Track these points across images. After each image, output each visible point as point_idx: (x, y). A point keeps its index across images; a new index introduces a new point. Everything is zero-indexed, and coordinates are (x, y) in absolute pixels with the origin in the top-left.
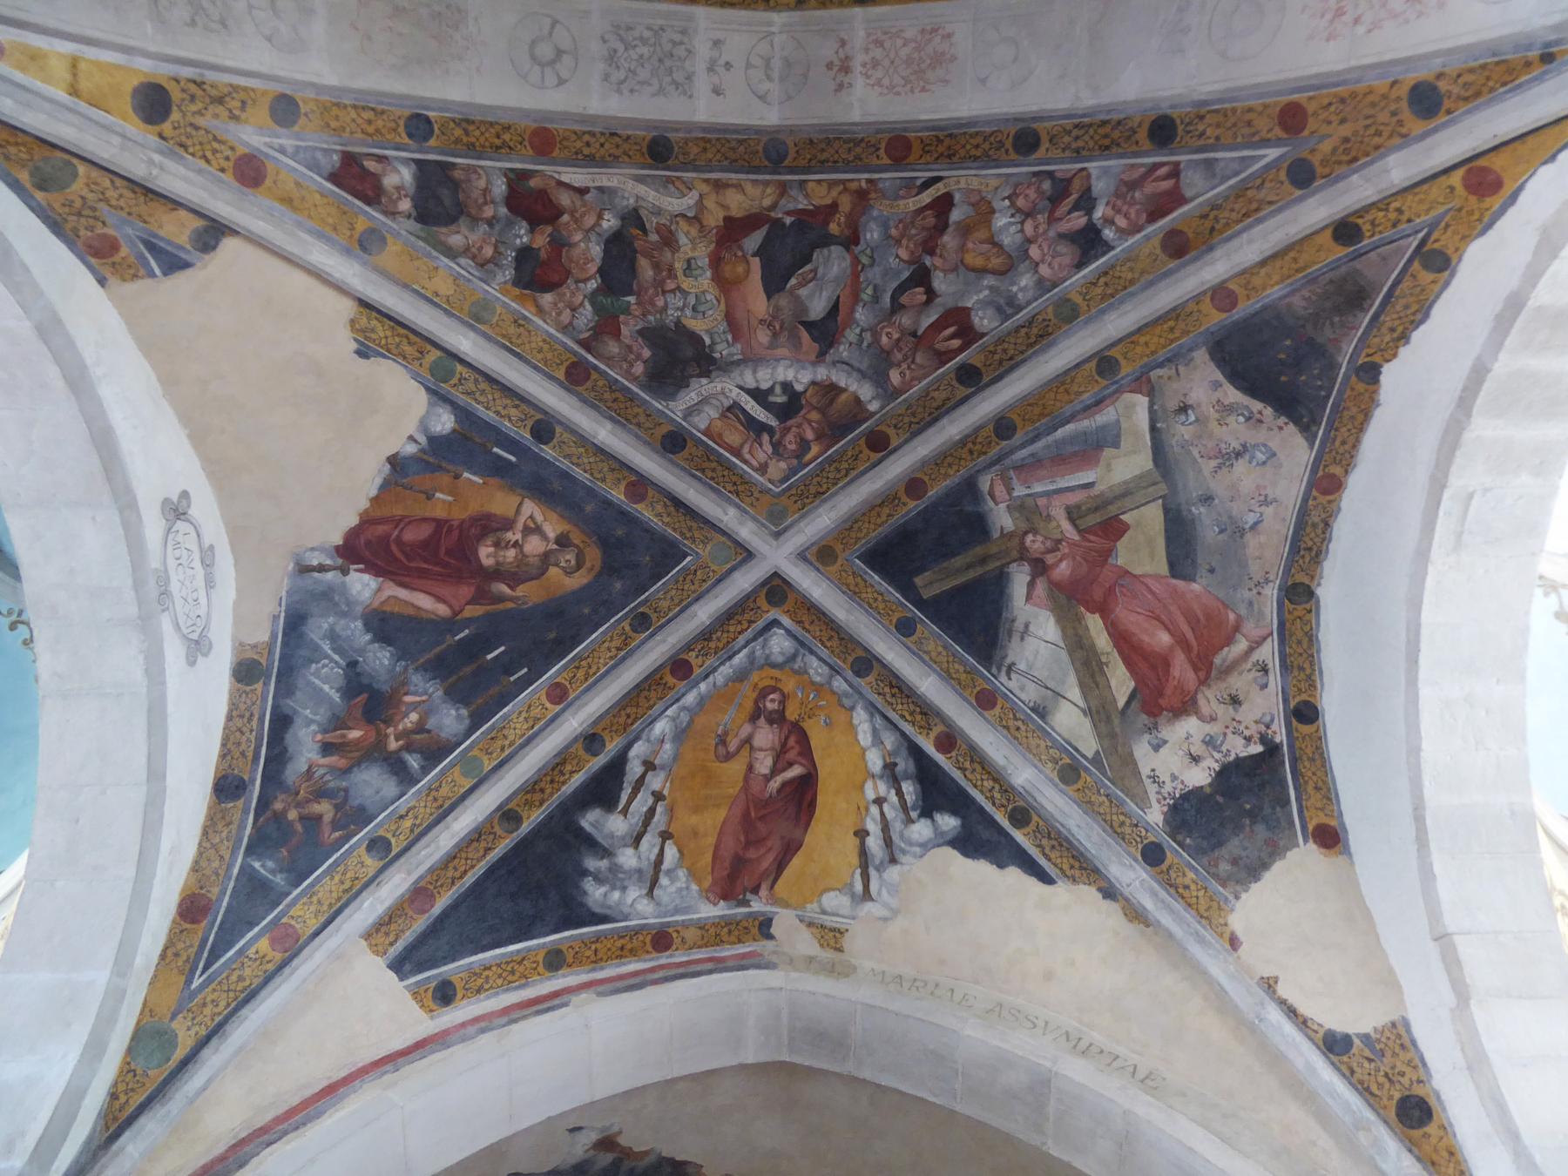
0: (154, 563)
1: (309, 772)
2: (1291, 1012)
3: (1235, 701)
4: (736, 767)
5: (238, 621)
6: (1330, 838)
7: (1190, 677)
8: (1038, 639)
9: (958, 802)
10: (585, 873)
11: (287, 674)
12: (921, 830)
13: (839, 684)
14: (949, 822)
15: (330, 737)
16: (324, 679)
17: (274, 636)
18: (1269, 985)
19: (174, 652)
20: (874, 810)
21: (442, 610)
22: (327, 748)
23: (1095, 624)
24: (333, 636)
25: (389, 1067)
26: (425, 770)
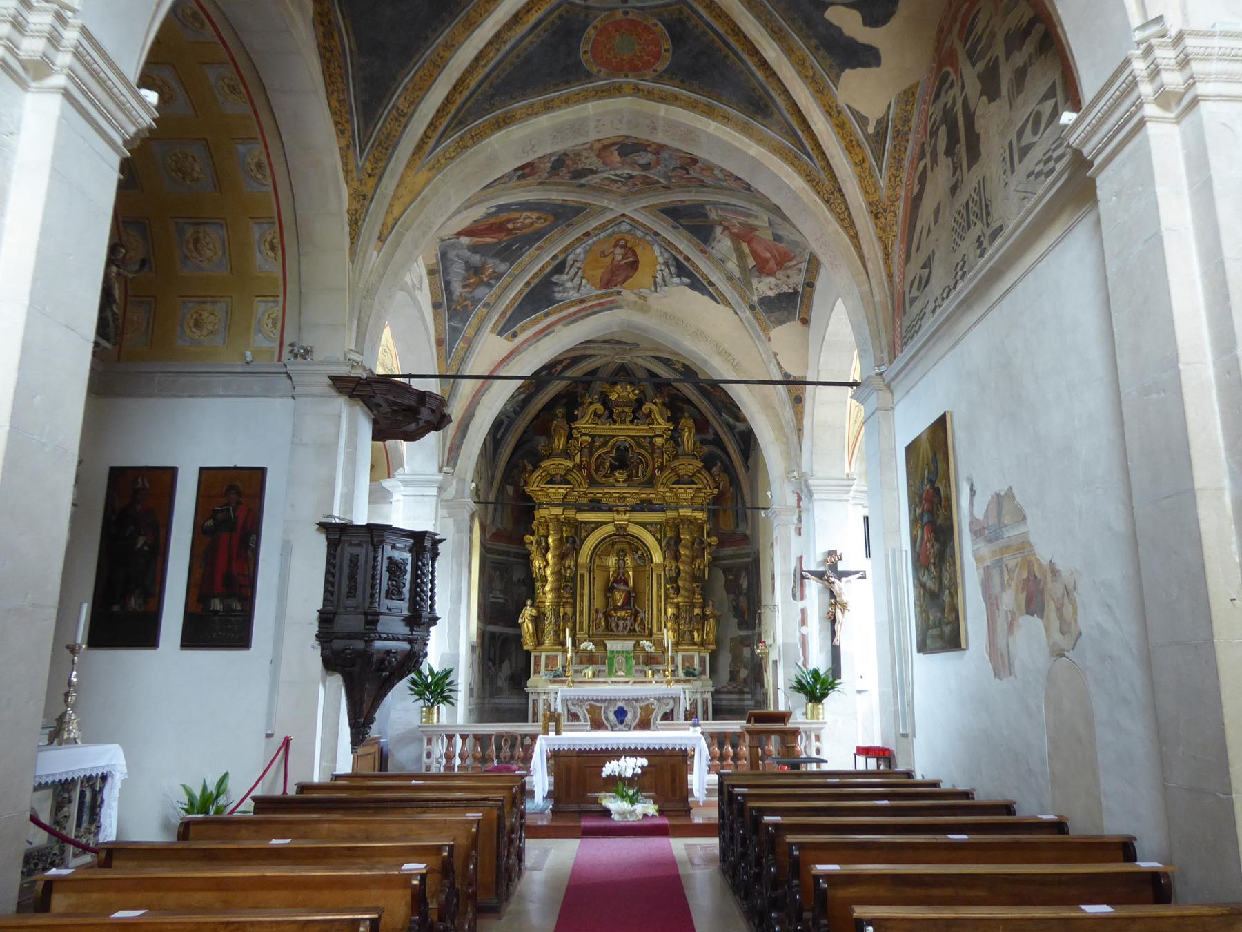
2: (779, 364)
4: (608, 259)
6: (805, 322)
8: (723, 244)
9: (690, 275)
11: (446, 271)
12: (677, 280)
13: (648, 238)
14: (687, 280)
16: (458, 269)
18: (775, 354)
22: (464, 287)
23: (745, 247)
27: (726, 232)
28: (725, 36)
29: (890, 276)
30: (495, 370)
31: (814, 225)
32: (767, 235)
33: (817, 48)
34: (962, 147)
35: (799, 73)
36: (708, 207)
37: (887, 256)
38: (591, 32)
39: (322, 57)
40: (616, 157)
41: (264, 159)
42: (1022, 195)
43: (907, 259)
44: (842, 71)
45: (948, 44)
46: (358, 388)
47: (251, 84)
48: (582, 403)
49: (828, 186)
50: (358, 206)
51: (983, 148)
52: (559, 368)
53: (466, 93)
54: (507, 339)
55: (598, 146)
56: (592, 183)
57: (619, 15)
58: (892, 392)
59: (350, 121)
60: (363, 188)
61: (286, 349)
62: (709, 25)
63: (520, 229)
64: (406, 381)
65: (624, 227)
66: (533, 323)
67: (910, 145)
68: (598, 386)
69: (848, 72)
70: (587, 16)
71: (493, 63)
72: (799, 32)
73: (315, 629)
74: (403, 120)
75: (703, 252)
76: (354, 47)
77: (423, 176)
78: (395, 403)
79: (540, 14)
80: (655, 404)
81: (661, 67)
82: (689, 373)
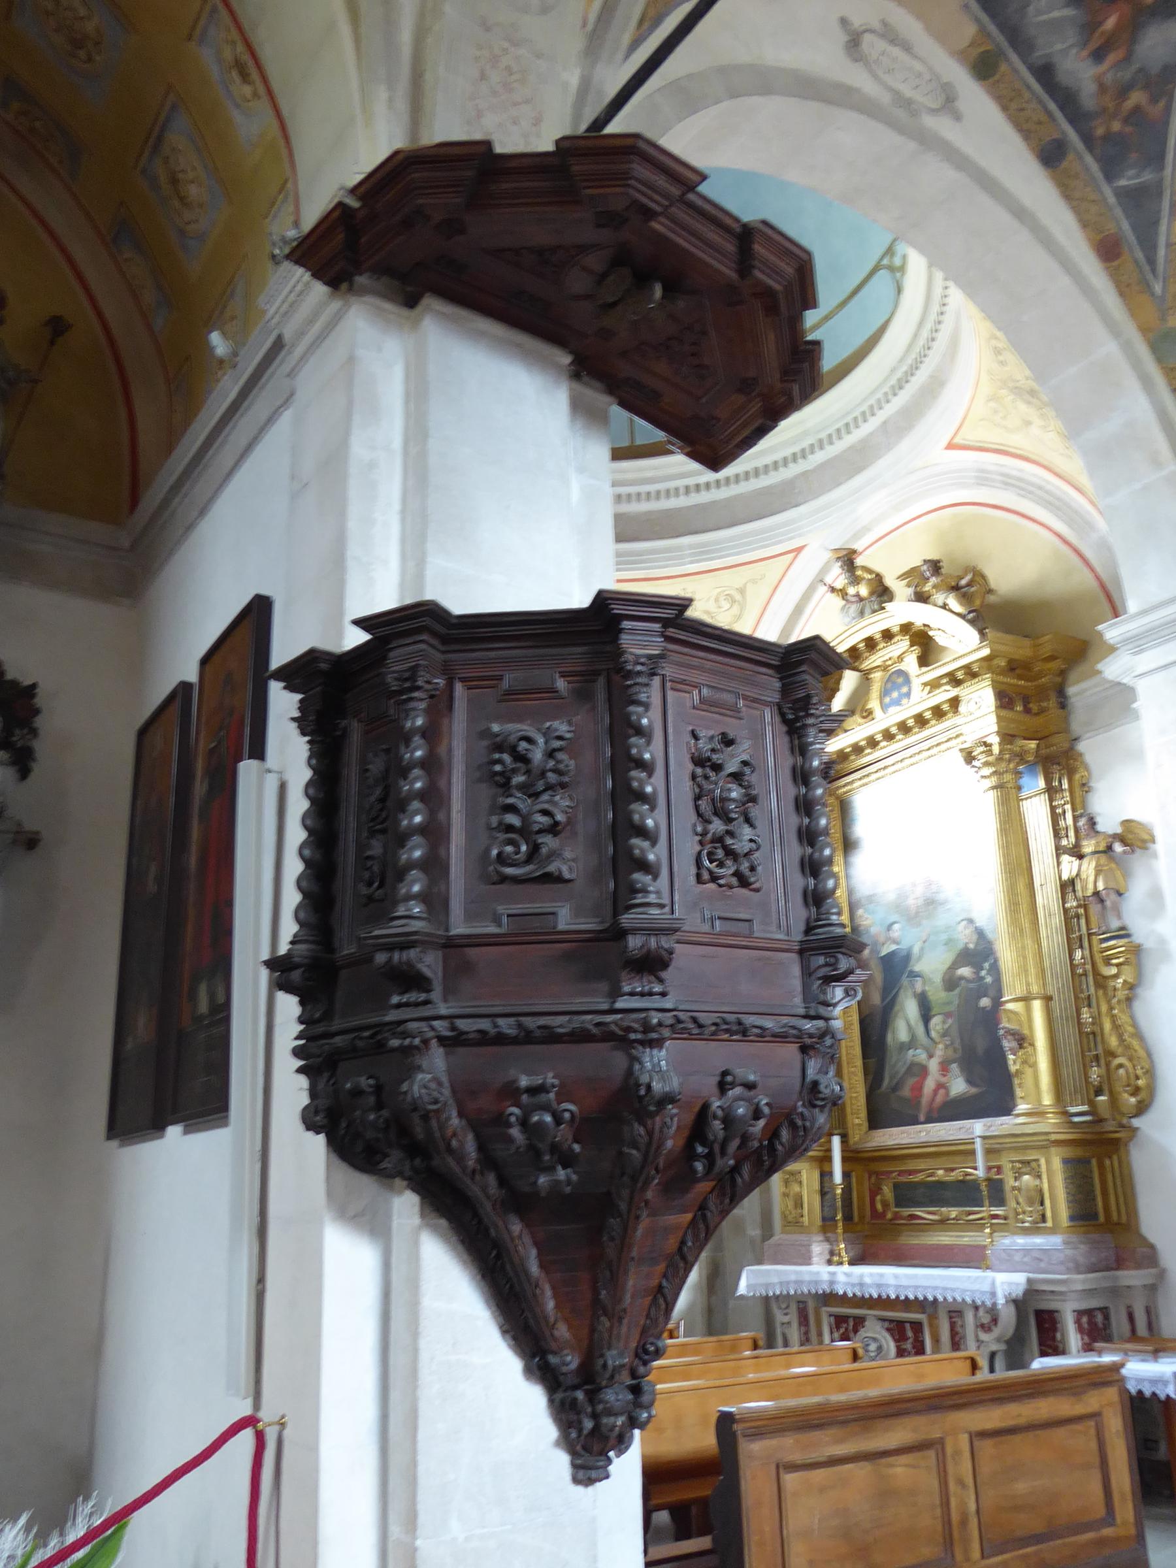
0: (886, 99)
5: (941, 37)
15: (1095, 43)
17: (977, 20)
19: (943, 127)
22: (1098, 55)
73: (551, 1431)
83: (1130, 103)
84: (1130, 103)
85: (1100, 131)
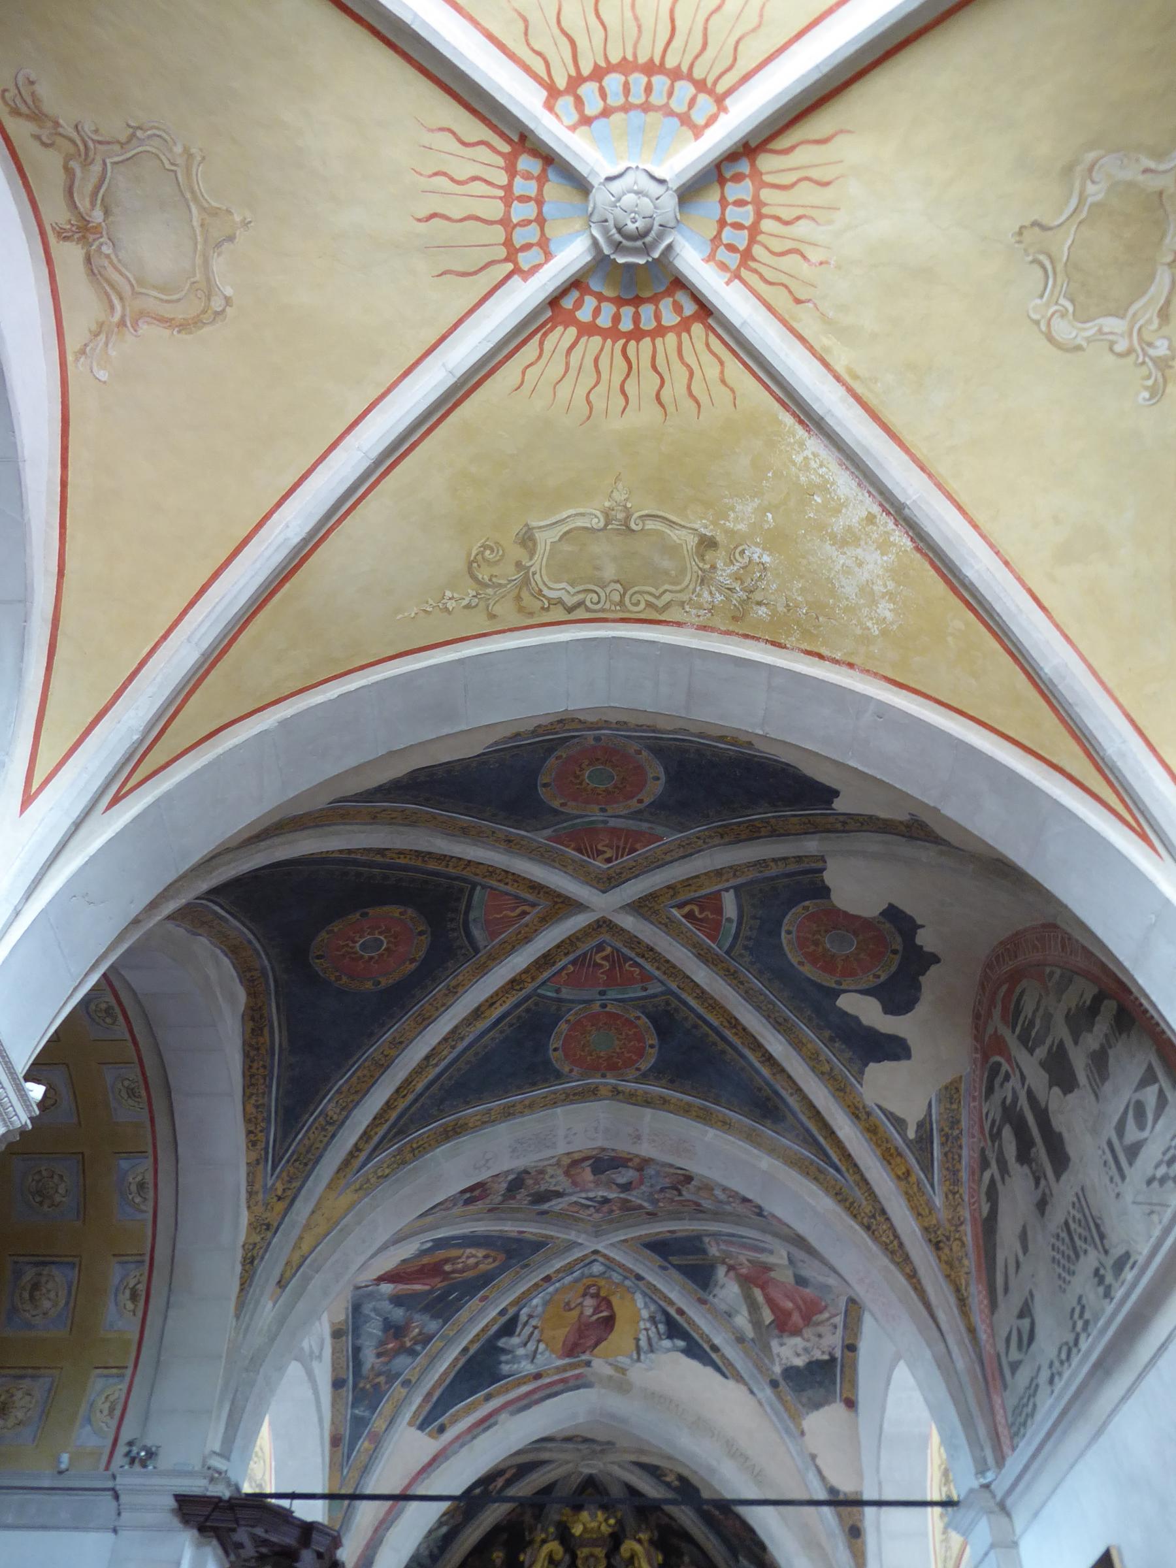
1: (373, 1367)
2: (819, 1472)
3: (820, 1336)
4: (575, 1314)
6: (851, 1404)
7: (800, 1322)
8: (729, 1291)
9: (683, 1334)
10: (500, 1363)
11: (356, 1331)
12: (667, 1343)
13: (627, 1283)
14: (681, 1344)
15: (380, 1350)
16: (374, 1328)
18: (813, 1457)
20: (644, 1332)
21: (427, 1288)
22: (379, 1355)
23: (758, 1294)
24: (374, 1310)
25: (424, 1475)
26: (424, 1348)
27: (732, 1274)
28: (721, 1029)
29: (972, 1330)
30: (409, 1485)
31: (853, 1261)
32: (785, 1276)
33: (832, 1039)
34: (1040, 1151)
35: (813, 1069)
36: (706, 1240)
37: (962, 1302)
38: (563, 1027)
39: (246, 1055)
40: (587, 1175)
41: (149, 1177)
42: (1147, 1209)
43: (993, 1305)
44: (866, 1065)
45: (990, 1030)
46: (216, 1515)
47: (155, 1088)
48: (531, 1542)
49: (867, 1208)
50: (258, 1239)
51: (1071, 1150)
52: (500, 1482)
53: (411, 1097)
54: (430, 1435)
55: (566, 1161)
56: (557, 1209)
57: (596, 1008)
58: (1008, 1515)
59: (266, 1130)
60: (268, 1214)
61: (122, 1449)
62: (700, 1017)
63: (462, 1271)
64: (285, 1503)
65: (597, 1268)
66: (469, 1410)
67: (965, 1152)
68: (555, 1513)
69: (872, 1067)
70: (559, 1009)
71: (446, 1061)
72: (809, 1022)
74: (331, 1129)
75: (703, 1302)
76: (285, 1044)
77: (347, 1197)
78: (265, 1542)
79: (506, 1007)
80: (639, 1541)
81: (645, 1065)
82: (686, 1489)
83: (377, 1380)
84: (377, 1380)
85: (361, 1385)
